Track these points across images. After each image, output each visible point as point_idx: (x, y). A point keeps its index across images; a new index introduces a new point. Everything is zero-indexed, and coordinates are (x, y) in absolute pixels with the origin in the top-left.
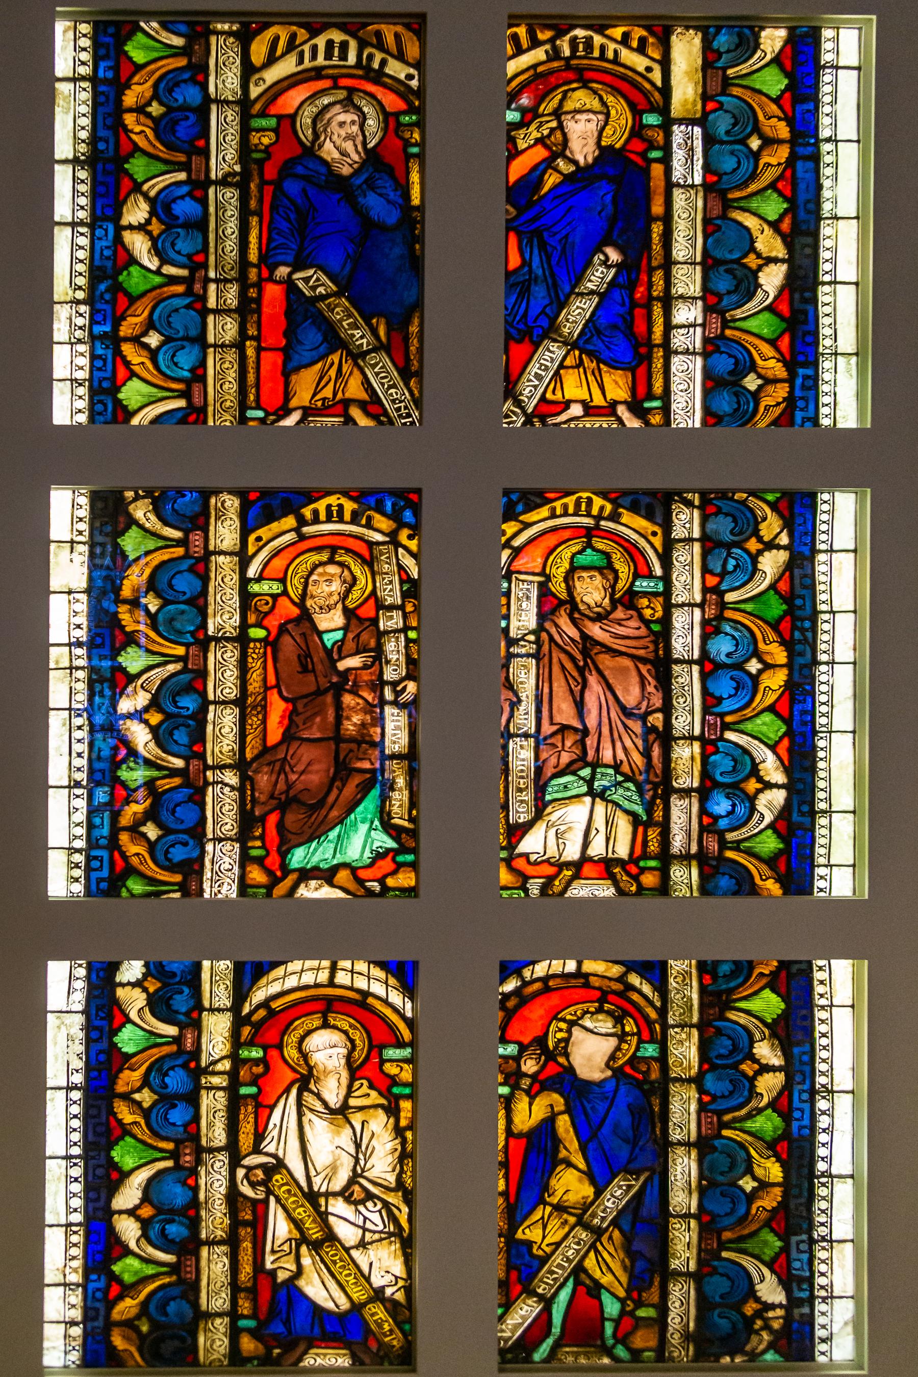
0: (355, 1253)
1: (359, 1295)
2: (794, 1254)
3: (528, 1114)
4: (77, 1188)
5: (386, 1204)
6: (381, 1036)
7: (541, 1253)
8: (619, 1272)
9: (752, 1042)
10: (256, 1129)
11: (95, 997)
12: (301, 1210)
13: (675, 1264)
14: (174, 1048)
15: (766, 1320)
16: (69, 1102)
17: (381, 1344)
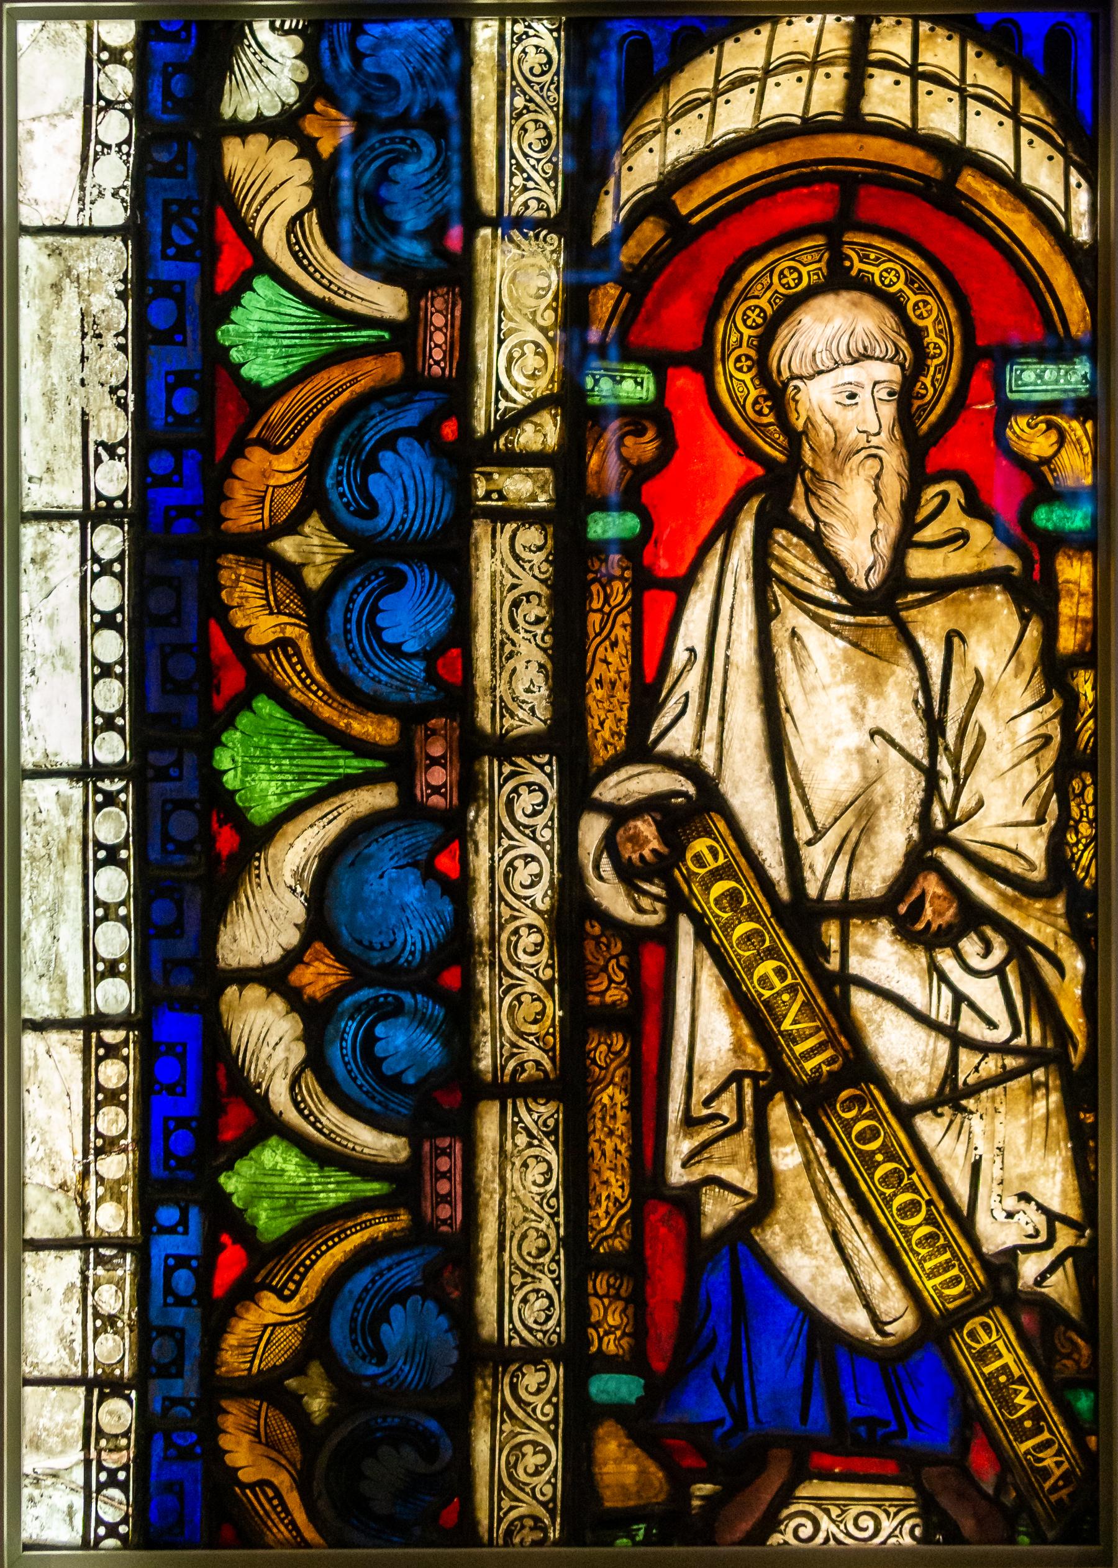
0: (929, 1128)
1: (942, 1287)
4: (113, 884)
5: (1018, 942)
6: (1002, 317)
10: (637, 669)
11: (165, 171)
12: (768, 967)
14: (392, 366)
16: (91, 567)
17: (1006, 1463)
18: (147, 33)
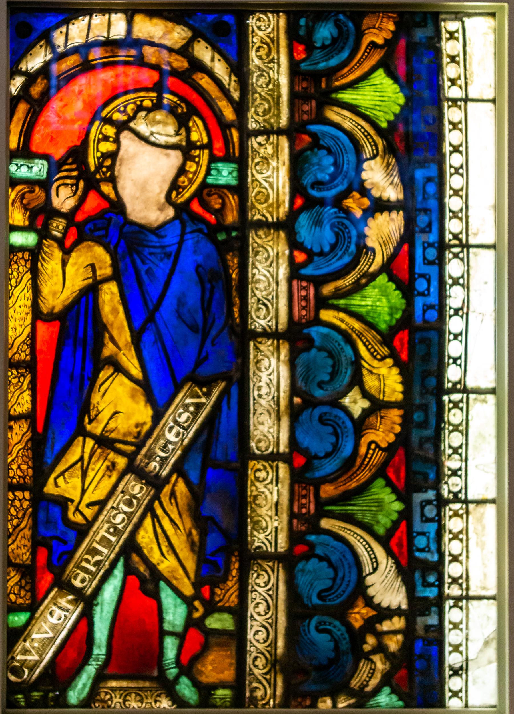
2: (418, 526)
3: (63, 278)
7: (79, 519)
8: (185, 553)
9: (360, 161)
13: (259, 539)
15: (380, 635)
18: (441, 703)
